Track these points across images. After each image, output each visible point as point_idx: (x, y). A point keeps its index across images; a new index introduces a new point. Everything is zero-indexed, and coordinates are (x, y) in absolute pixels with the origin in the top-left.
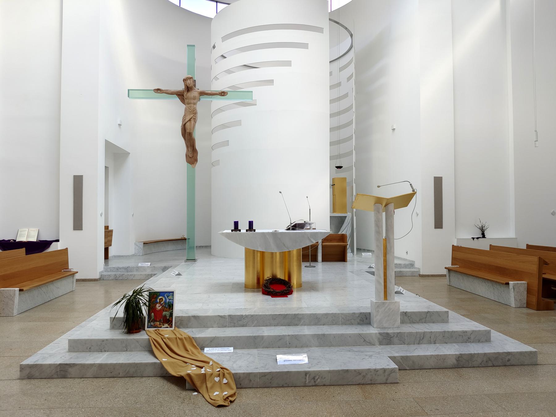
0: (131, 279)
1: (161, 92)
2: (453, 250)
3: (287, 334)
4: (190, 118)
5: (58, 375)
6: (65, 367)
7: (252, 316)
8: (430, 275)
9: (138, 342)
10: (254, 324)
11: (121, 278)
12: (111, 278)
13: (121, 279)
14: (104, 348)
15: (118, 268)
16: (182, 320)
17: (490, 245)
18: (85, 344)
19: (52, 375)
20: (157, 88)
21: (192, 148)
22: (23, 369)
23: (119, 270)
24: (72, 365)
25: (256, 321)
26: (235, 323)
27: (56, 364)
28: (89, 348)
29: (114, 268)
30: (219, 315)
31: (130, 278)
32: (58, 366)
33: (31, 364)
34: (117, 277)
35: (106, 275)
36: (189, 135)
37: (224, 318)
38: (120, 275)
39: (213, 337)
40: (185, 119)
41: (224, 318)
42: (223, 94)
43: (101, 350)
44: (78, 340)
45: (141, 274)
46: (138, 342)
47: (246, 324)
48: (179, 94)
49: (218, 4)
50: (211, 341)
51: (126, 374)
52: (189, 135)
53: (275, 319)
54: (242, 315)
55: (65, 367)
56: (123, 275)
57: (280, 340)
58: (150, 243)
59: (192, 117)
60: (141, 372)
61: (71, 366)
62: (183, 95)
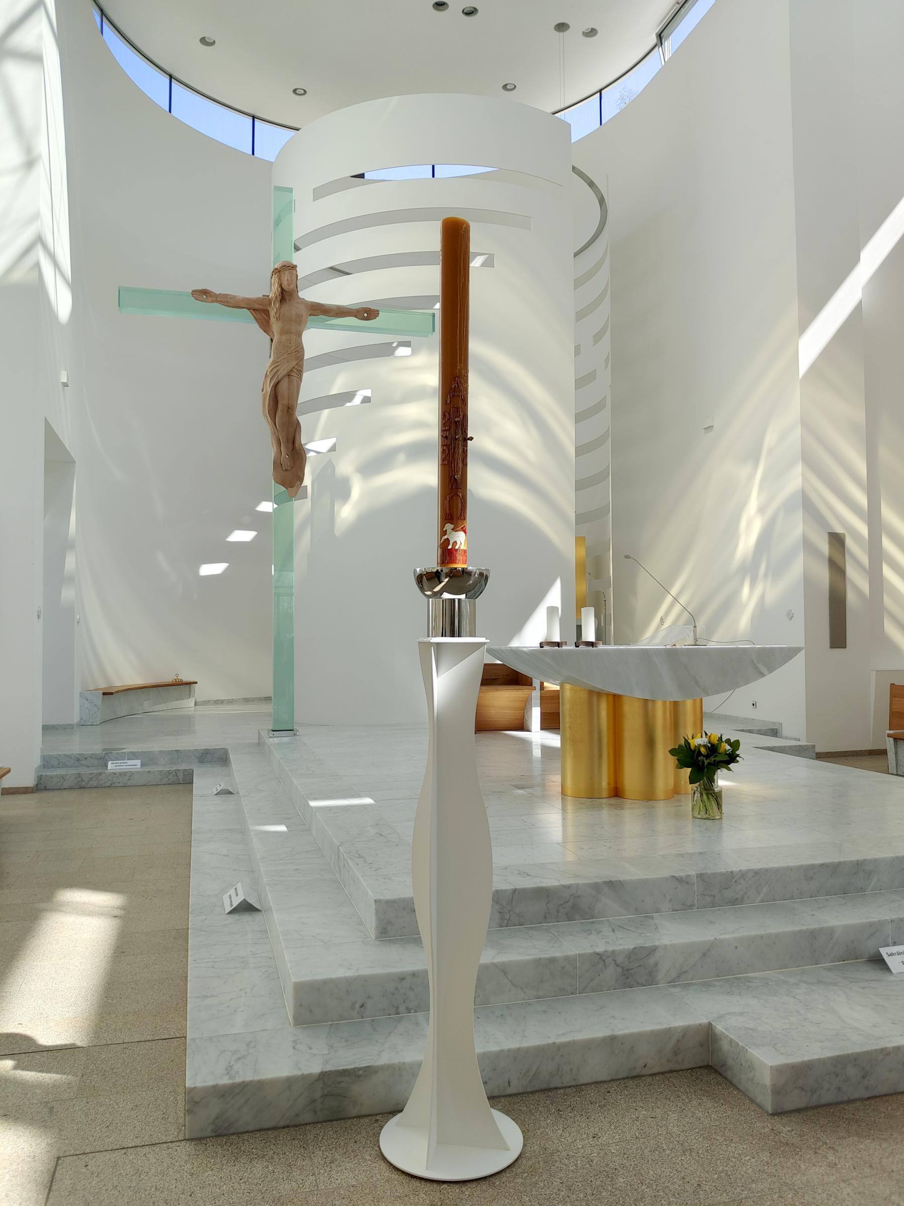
0: (120, 785)
1: (210, 299)
2: (893, 696)
3: (888, 918)
4: (290, 368)
5: (315, 1112)
6: (339, 1083)
7: (756, 873)
8: (823, 753)
9: (505, 972)
10: (762, 895)
11: (94, 783)
12: (66, 785)
13: (95, 785)
14: (404, 1002)
15: (80, 757)
16: (579, 897)
17: (892, 685)
18: (348, 992)
19: (297, 1115)
20: (200, 288)
21: (291, 446)
22: (197, 1103)
23: (81, 762)
24: (360, 1072)
25: (767, 886)
26: (714, 896)
27: (309, 1076)
28: (358, 1006)
29: (69, 756)
30: (674, 877)
31: (119, 783)
32: (316, 1080)
33: (225, 1086)
34: (82, 780)
35: (52, 777)
36: (288, 412)
37: (687, 883)
38: (91, 776)
39: (710, 940)
40: (278, 371)
41: (687, 883)
42: (366, 315)
43: (397, 1008)
44: (325, 982)
45: (149, 772)
46: (505, 972)
47: (742, 898)
48: (257, 306)
49: (257, 122)
50: (704, 955)
51: (530, 1081)
52: (285, 411)
53: (812, 878)
54: (732, 872)
55: (339, 1083)
56: (101, 774)
57: (872, 935)
58: (125, 690)
59: (294, 367)
60: (571, 1070)
61: (359, 1076)
62: (267, 313)
